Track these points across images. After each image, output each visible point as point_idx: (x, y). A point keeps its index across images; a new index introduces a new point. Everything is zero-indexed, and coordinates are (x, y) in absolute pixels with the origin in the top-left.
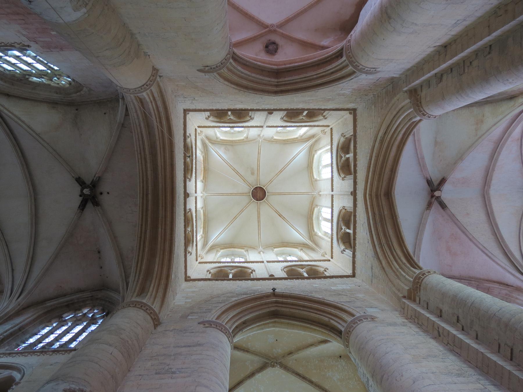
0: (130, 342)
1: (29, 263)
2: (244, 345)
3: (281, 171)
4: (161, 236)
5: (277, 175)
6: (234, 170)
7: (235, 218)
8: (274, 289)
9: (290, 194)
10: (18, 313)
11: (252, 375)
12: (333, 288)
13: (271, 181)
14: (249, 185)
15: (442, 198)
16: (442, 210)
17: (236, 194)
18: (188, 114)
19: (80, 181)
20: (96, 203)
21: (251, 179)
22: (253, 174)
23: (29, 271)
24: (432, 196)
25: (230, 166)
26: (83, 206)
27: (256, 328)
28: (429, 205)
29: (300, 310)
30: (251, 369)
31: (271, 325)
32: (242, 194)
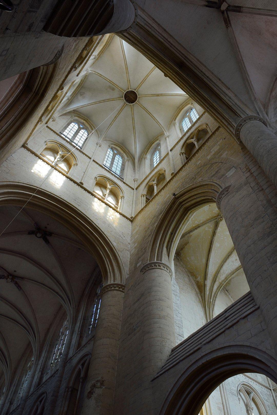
0: (110, 324)
1: (59, 285)
2: (194, 225)
3: (127, 68)
4: (87, 234)
5: (127, 73)
6: (100, 102)
7: (134, 128)
8: (174, 195)
9: (148, 76)
10: (78, 311)
11: (214, 233)
12: (209, 157)
13: (129, 81)
14: (120, 98)
15: (231, 4)
16: (240, 14)
17: (119, 114)
18: (27, 144)
19: (31, 233)
20: (51, 234)
21: (116, 94)
22: (113, 89)
23: (63, 289)
24: (223, 12)
25: (95, 103)
26: (47, 241)
27: (183, 226)
28: (227, 22)
29: (195, 199)
30: (211, 230)
31: (190, 216)
32: (121, 110)
